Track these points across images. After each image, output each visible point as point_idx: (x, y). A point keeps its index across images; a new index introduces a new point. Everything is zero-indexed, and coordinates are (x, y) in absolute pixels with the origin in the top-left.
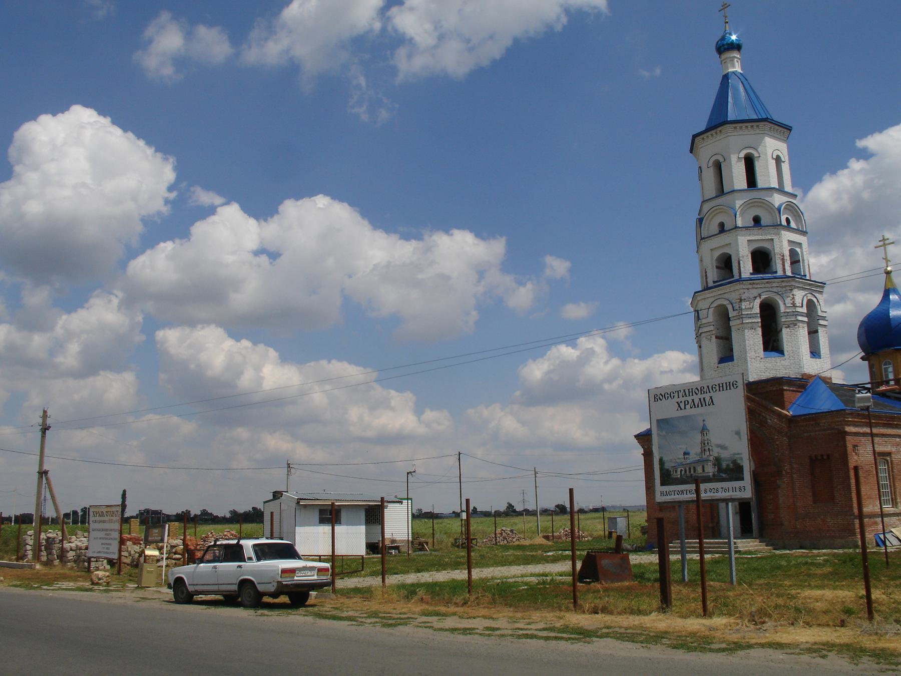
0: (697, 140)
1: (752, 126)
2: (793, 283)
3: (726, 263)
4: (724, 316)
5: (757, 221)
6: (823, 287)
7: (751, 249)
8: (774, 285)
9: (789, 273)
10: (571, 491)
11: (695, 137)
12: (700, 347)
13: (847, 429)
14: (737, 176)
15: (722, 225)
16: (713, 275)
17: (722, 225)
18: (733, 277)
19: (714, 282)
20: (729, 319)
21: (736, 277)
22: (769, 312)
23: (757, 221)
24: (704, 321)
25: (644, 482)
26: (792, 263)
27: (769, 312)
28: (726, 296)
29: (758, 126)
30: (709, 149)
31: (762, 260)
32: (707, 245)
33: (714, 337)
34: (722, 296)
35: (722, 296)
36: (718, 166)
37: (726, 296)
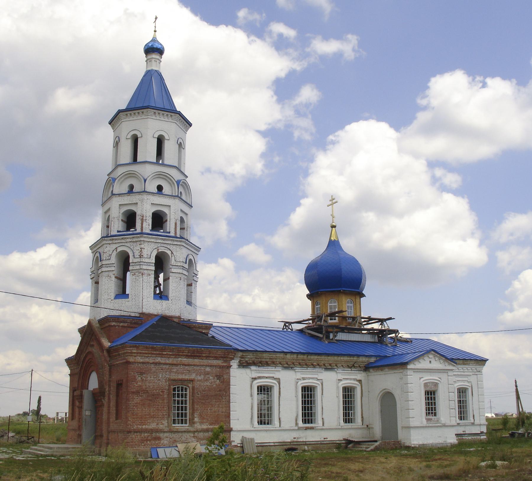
0: (120, 114)
1: (139, 113)
2: (142, 239)
3: (130, 219)
4: (125, 262)
5: (160, 188)
6: (199, 251)
7: (153, 211)
8: (128, 240)
9: (178, 236)
10: (40, 398)
11: (120, 111)
12: (97, 283)
13: (131, 359)
14: (147, 150)
15: (131, 187)
16: (117, 226)
17: (131, 187)
18: (136, 230)
19: (118, 231)
20: (129, 264)
21: (139, 230)
22: (161, 263)
23: (160, 188)
24: (104, 263)
25: (68, 394)
26: (181, 229)
27: (161, 263)
28: (171, 247)
29: (171, 116)
30: (129, 126)
31: (159, 220)
32: (115, 203)
33: (113, 277)
34: (126, 244)
35: (126, 244)
36: (135, 140)
37: (171, 247)
